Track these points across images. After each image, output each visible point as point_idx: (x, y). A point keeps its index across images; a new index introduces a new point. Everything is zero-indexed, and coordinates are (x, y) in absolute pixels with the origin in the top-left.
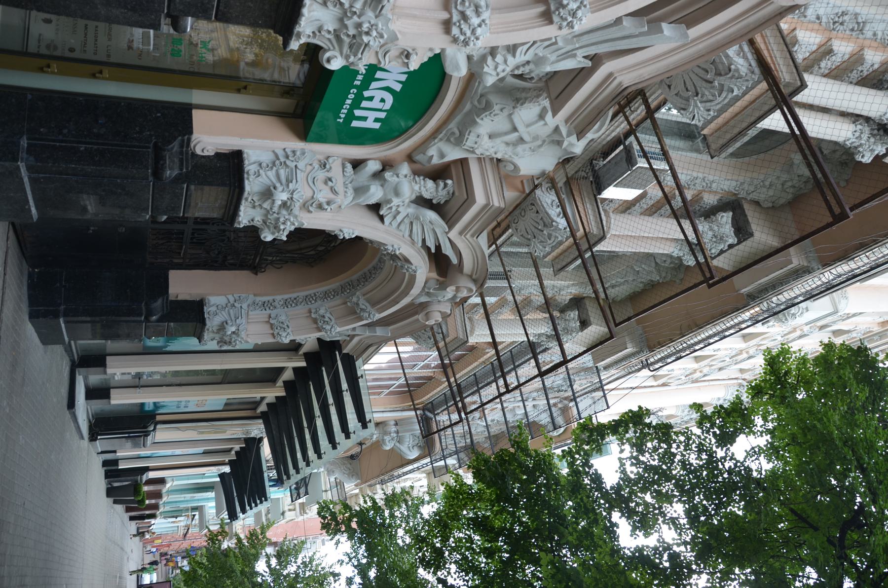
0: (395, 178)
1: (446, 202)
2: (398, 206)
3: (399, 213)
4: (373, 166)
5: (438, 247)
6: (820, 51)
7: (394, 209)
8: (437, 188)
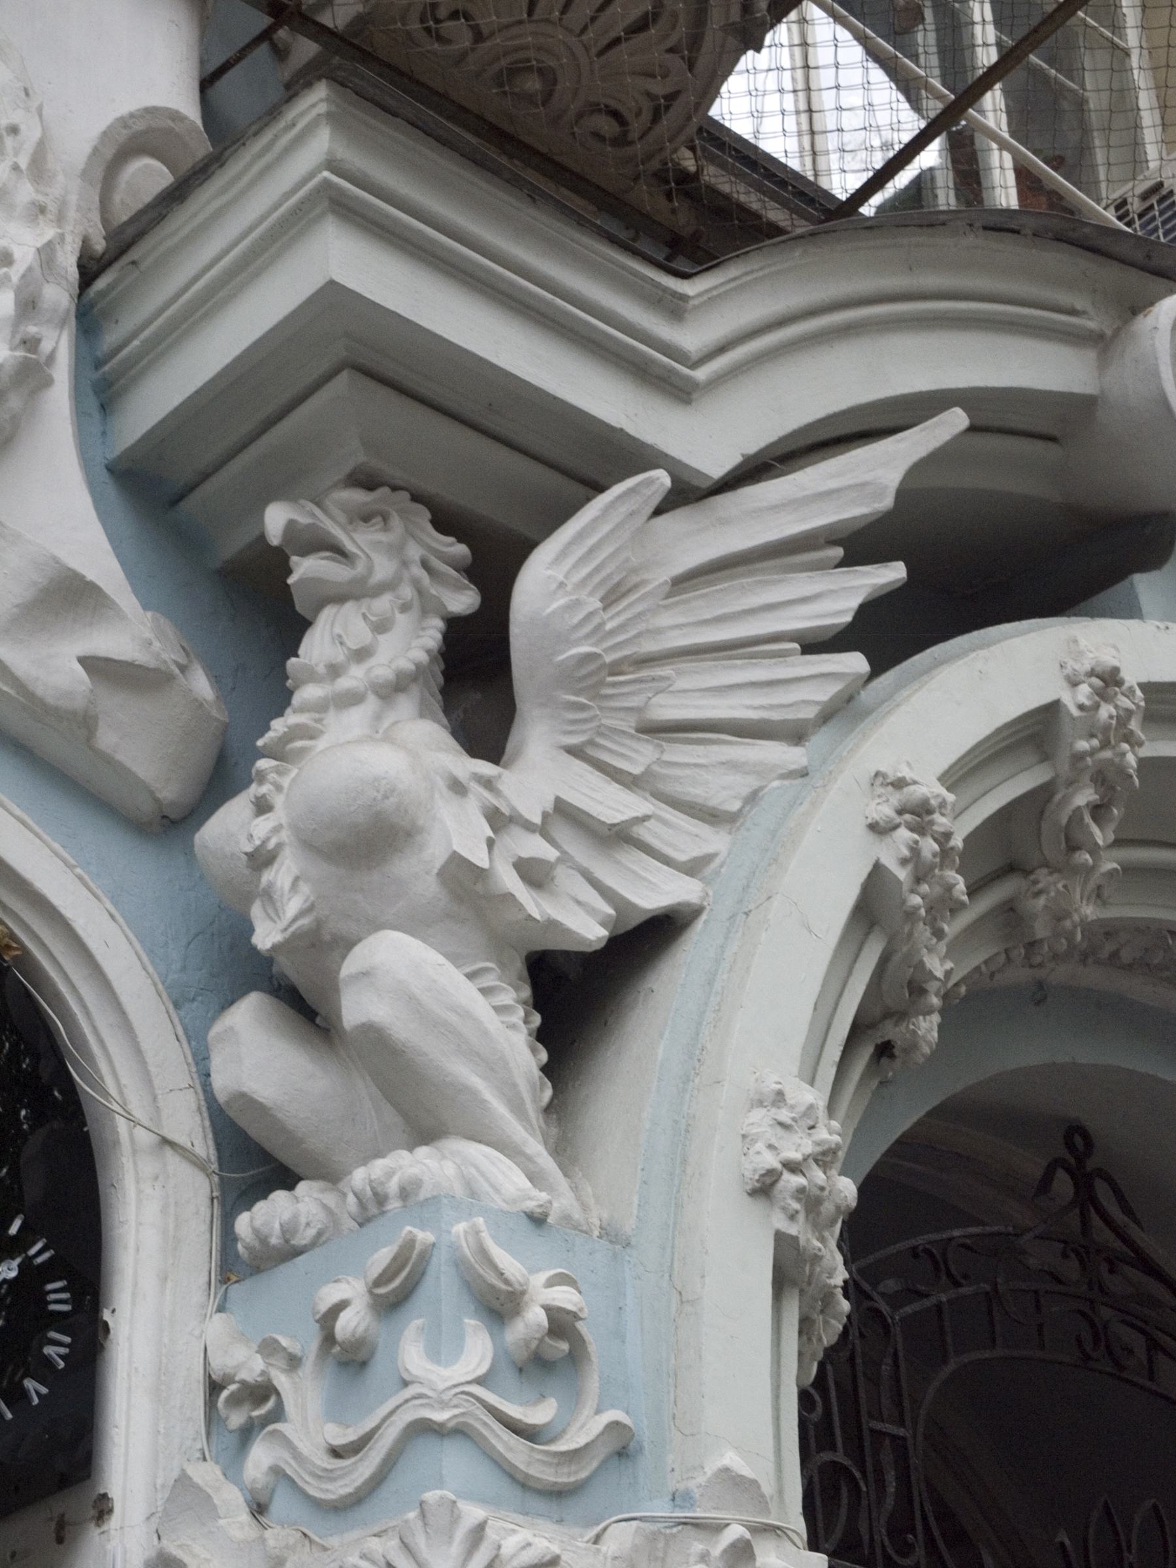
0: (280, 875)
1: (446, 521)
2: (499, 820)
3: (563, 811)
4: (255, 1054)
5: (859, 545)
6: (623, 235)
7: (536, 847)
8: (339, 597)
